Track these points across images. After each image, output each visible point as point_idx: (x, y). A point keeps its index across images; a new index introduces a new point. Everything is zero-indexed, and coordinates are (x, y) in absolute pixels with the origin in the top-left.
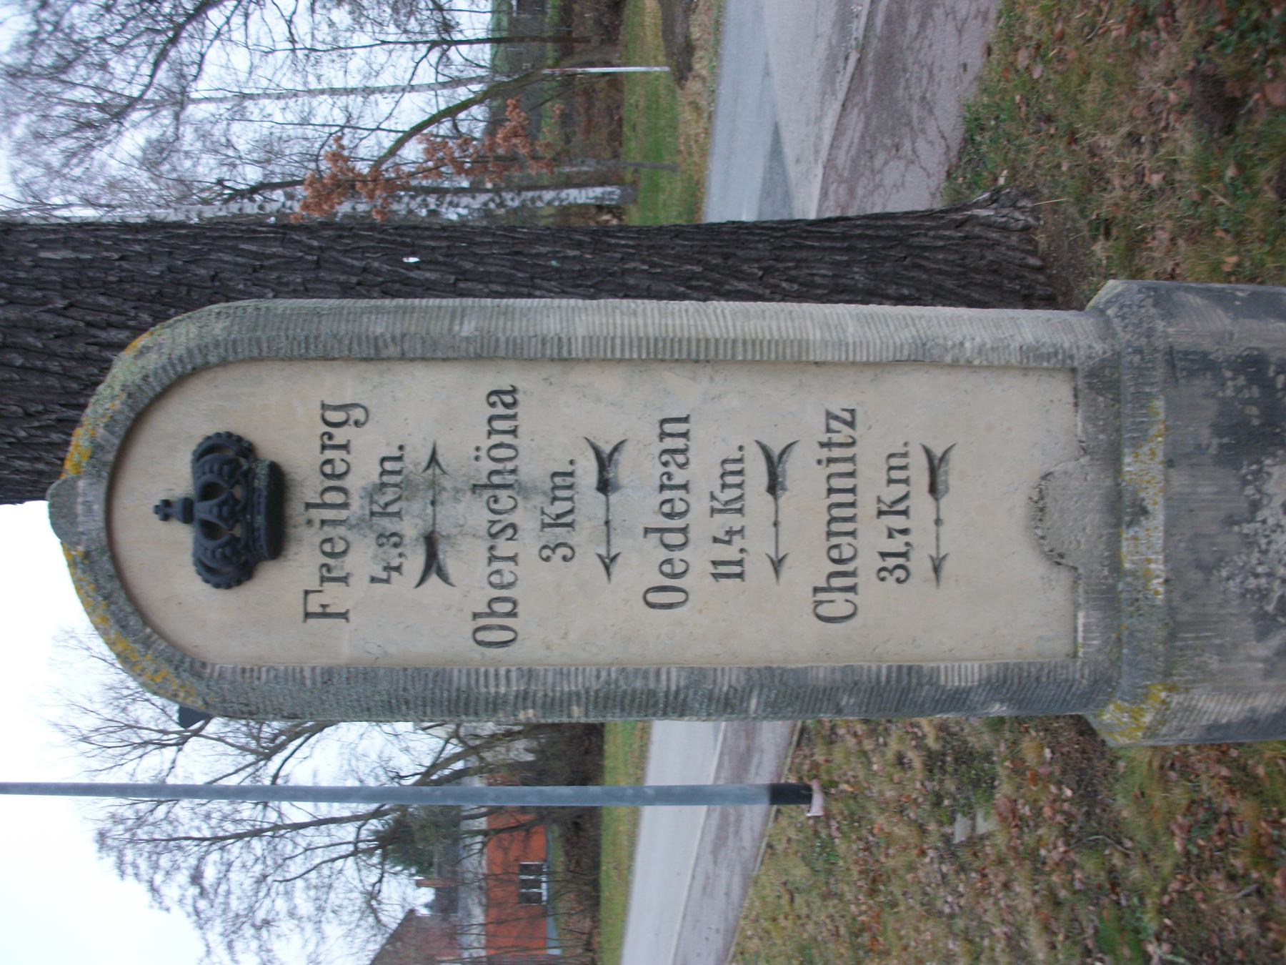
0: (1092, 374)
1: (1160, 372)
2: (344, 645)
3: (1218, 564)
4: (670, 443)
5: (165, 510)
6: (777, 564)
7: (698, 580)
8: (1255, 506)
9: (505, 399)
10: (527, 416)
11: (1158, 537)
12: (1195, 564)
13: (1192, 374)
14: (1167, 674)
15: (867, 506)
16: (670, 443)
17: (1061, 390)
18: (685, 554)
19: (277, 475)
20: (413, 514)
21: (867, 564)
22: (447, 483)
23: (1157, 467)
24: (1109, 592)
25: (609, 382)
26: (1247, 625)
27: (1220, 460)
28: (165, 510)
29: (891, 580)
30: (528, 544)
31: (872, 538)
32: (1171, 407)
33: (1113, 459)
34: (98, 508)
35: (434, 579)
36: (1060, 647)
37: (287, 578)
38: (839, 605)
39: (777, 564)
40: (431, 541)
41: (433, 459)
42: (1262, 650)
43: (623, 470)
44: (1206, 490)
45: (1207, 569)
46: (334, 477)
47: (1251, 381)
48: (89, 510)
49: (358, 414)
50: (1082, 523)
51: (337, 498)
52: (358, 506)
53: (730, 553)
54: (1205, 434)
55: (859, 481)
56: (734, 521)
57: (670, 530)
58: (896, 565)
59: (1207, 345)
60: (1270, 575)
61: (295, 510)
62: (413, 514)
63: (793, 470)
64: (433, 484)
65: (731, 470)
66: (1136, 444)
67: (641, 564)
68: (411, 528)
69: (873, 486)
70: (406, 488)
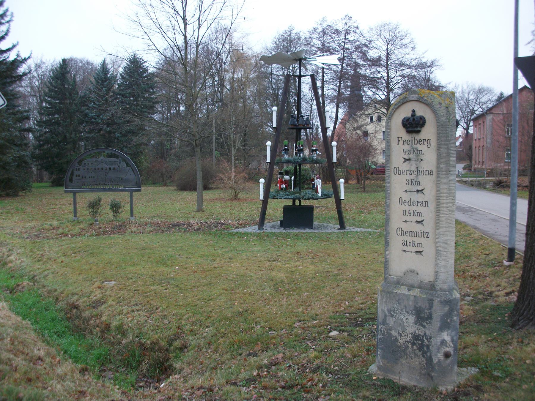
0: (434, 285)
1: (430, 297)
2: (394, 144)
3: (399, 303)
4: (424, 203)
5: (414, 111)
6: (405, 221)
7: (403, 207)
8: (408, 312)
9: (431, 173)
10: (429, 177)
11: (404, 292)
12: (399, 299)
13: (429, 304)
14: (383, 291)
15: (414, 239)
16: (424, 203)
17: (432, 279)
18: (407, 205)
19: (419, 132)
20: (414, 156)
21: (405, 238)
22: (418, 162)
23: (415, 294)
24: (398, 283)
25: (434, 192)
26: (389, 308)
27: (415, 307)
28: (414, 111)
29: (402, 242)
30: (409, 177)
31: (409, 239)
32: (424, 298)
33: (420, 287)
34: (413, 99)
35: (404, 160)
36: (391, 273)
37: (402, 133)
38: (399, 232)
39: (405, 221)
40: (409, 160)
41: (422, 160)
42: (386, 310)
43: (420, 194)
44: (411, 303)
45: (398, 301)
46: (419, 142)
47: (428, 316)
48: (413, 97)
49: (429, 146)
50: (410, 280)
51: (416, 143)
52: (415, 146)
53: (407, 213)
54: (419, 304)
55: (418, 238)
56: (412, 214)
57: (411, 203)
58: (405, 244)
59: (434, 308)
60: (397, 313)
61: (414, 135)
62: (414, 156)
63: (420, 225)
64: (418, 160)
65: (420, 214)
66: (420, 292)
67: (406, 197)
68: (411, 156)
69: (417, 240)
70: (417, 155)
